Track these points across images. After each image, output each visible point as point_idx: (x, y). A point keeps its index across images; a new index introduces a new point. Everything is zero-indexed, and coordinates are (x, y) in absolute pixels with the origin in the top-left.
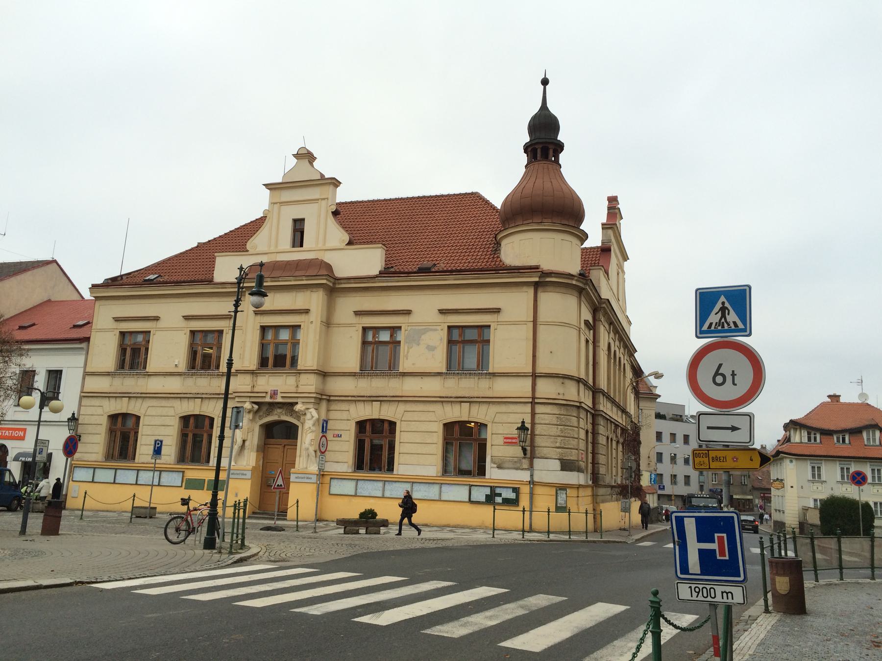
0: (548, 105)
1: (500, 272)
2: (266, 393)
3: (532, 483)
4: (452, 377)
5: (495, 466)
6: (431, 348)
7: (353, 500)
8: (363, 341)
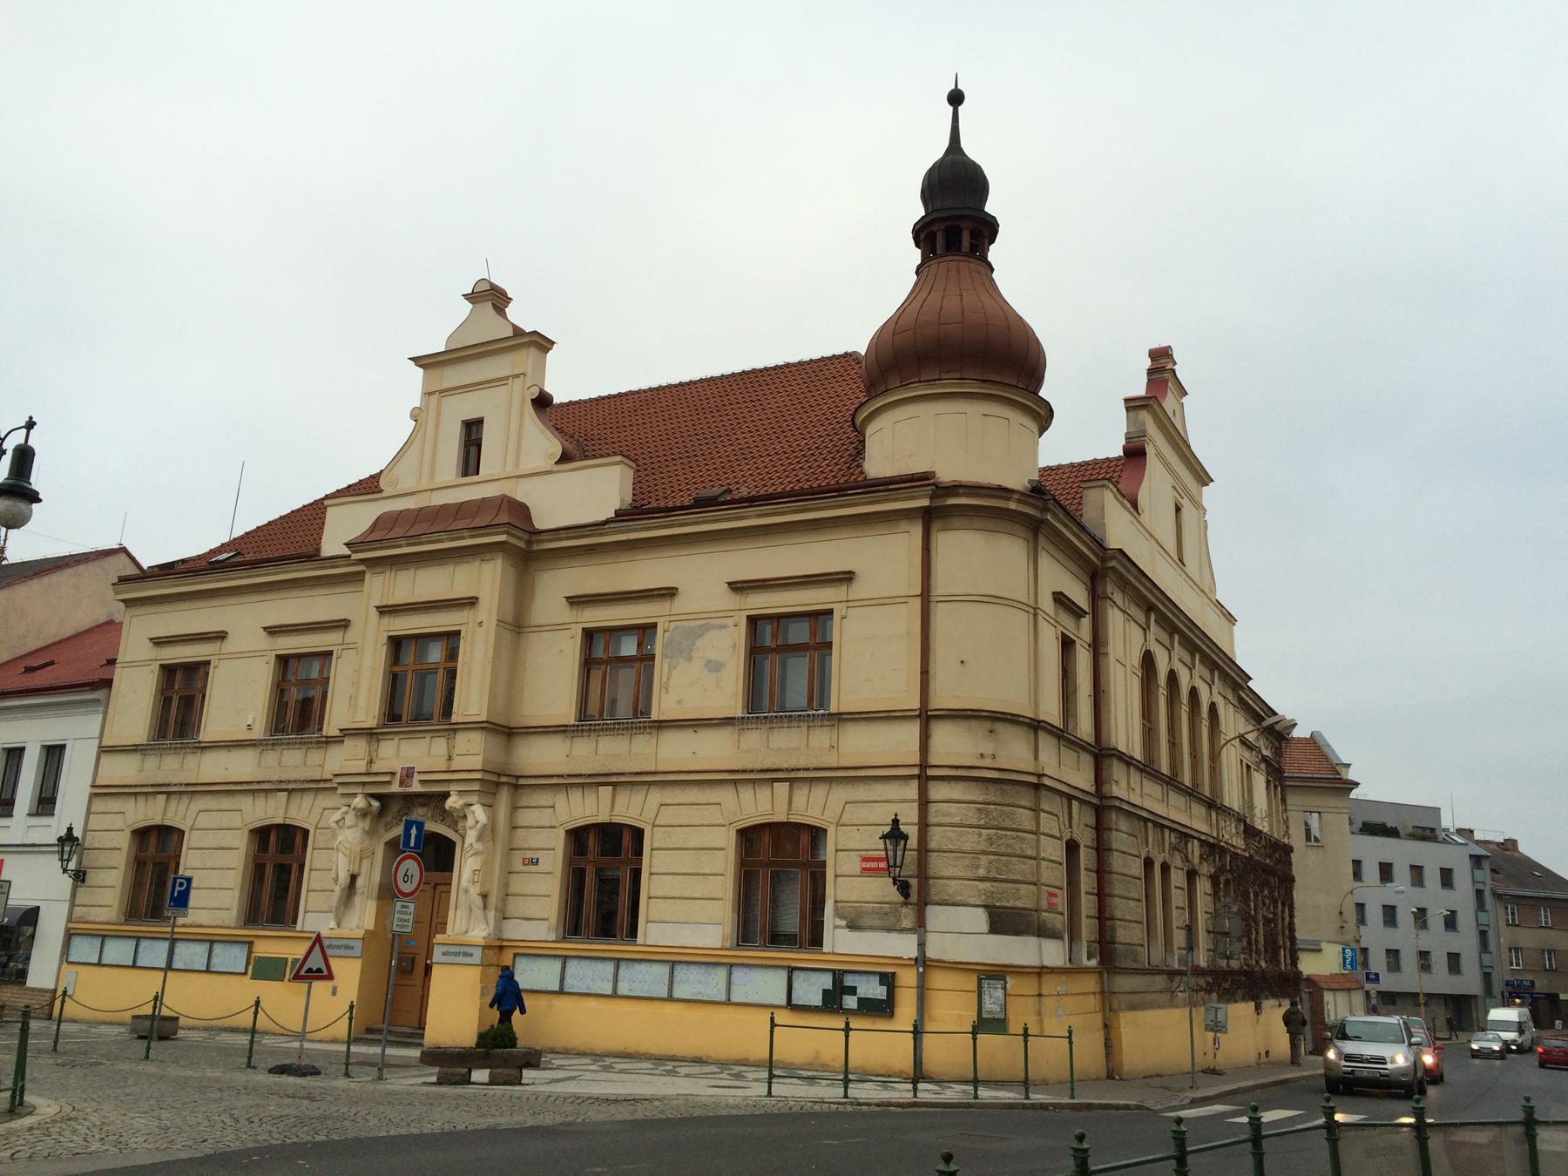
0: (963, 145)
1: (849, 492)
2: (393, 774)
3: (922, 962)
4: (754, 726)
5: (843, 923)
6: (714, 667)
7: (557, 1003)
8: (586, 659)
